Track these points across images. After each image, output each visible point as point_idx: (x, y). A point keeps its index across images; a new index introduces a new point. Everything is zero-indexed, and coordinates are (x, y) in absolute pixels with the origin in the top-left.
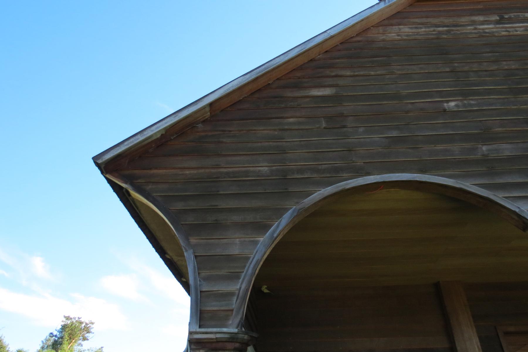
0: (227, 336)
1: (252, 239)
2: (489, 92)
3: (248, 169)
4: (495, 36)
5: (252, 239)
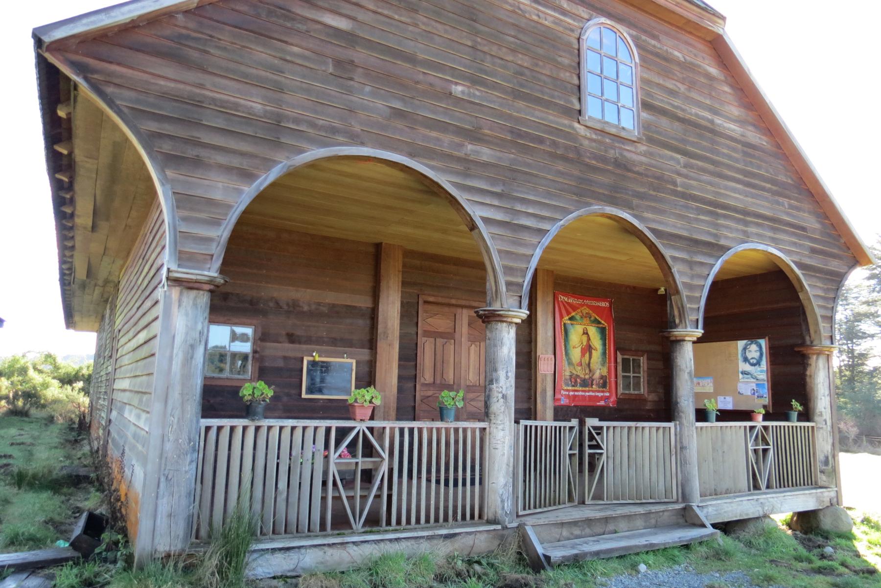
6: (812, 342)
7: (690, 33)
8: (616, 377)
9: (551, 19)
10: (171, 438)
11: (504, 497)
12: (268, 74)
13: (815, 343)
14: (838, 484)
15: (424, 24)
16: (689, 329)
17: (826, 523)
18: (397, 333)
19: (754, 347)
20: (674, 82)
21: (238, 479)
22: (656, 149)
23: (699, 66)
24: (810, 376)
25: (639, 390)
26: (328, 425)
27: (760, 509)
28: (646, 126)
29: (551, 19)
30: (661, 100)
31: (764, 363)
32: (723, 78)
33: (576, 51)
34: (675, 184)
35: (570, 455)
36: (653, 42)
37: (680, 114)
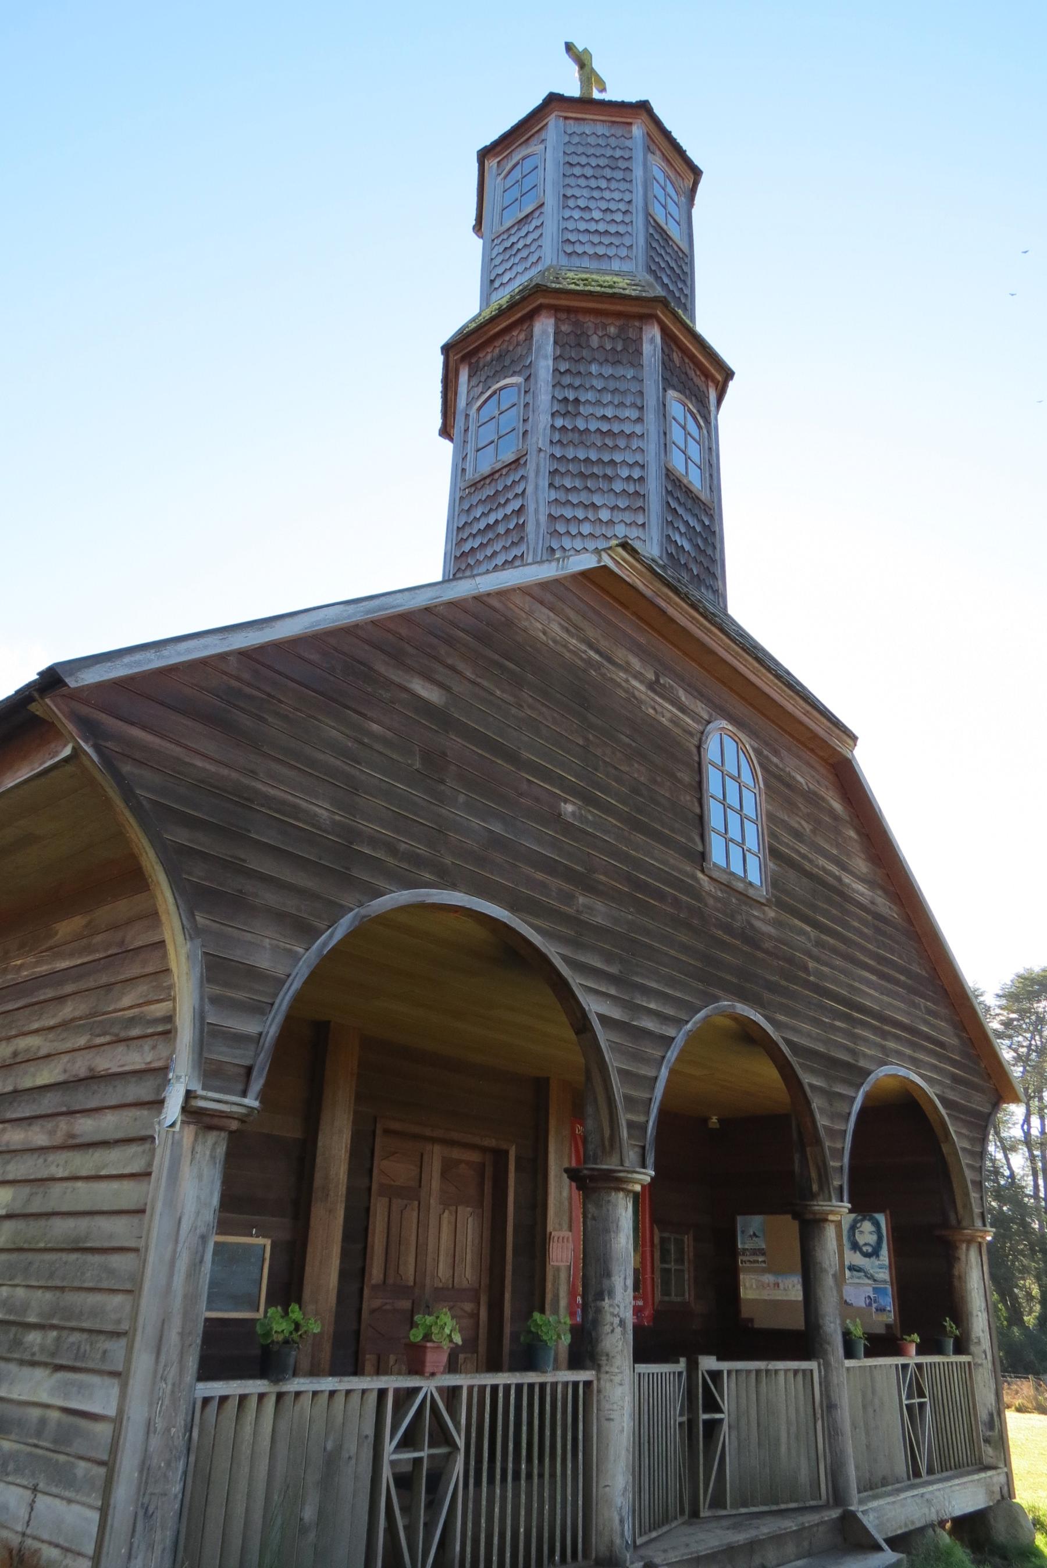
0: (243, 1110)
1: (288, 946)
2: (608, 809)
3: (298, 801)
4: (640, 708)
5: (288, 946)
6: (959, 1222)
7: (812, 750)
8: (653, 1272)
9: (668, 715)
10: (159, 1426)
11: (625, 1513)
12: (338, 763)
13: (964, 1224)
14: (1007, 1463)
15: (530, 707)
16: (834, 1202)
17: (1000, 1531)
18: (342, 1189)
19: (867, 1226)
20: (798, 819)
21: (366, 1508)
22: (786, 917)
23: (823, 799)
24: (960, 1277)
25: (683, 1295)
26: (382, 1386)
27: (926, 1511)
28: (775, 883)
29: (668, 715)
30: (789, 845)
31: (884, 1252)
32: (847, 818)
33: (696, 765)
34: (806, 969)
35: (680, 1424)
36: (775, 760)
37: (807, 866)
